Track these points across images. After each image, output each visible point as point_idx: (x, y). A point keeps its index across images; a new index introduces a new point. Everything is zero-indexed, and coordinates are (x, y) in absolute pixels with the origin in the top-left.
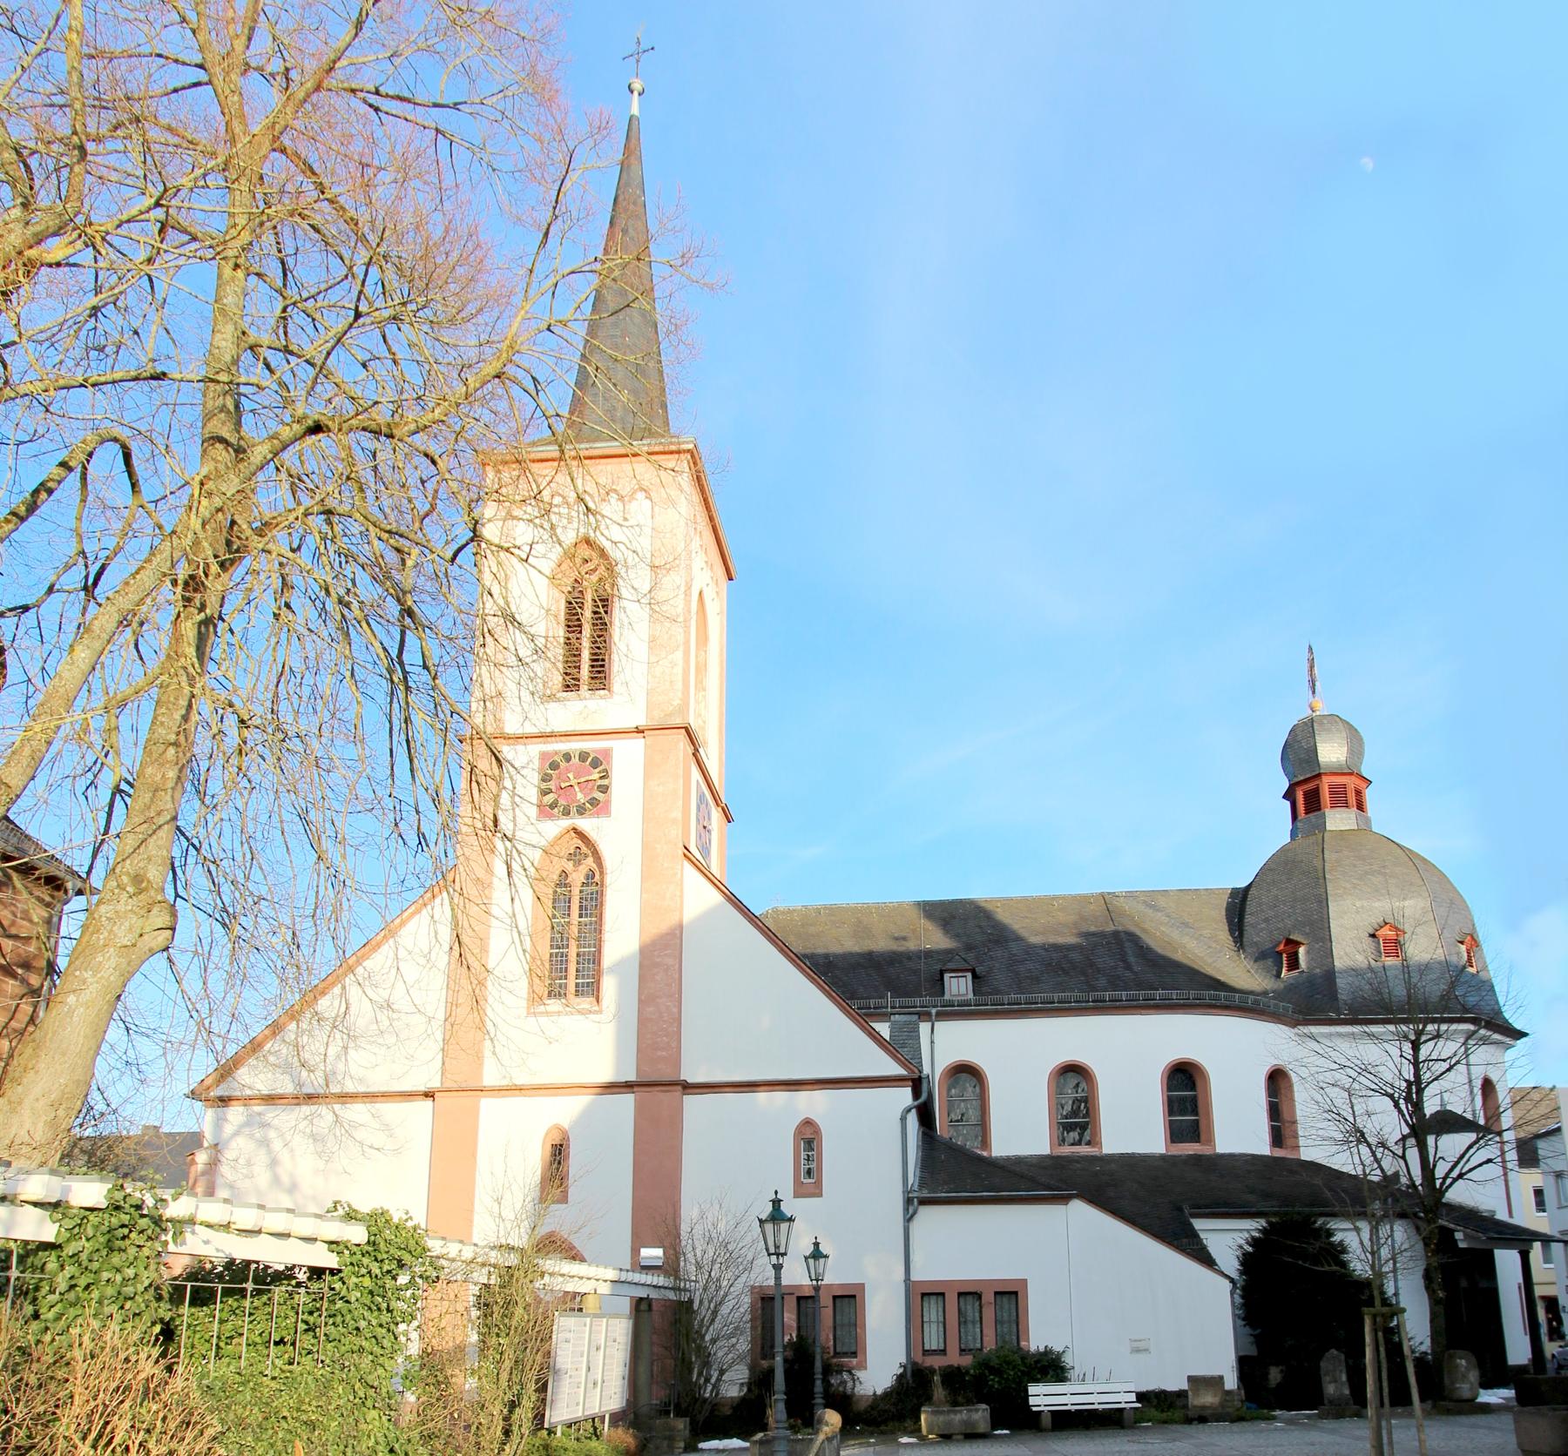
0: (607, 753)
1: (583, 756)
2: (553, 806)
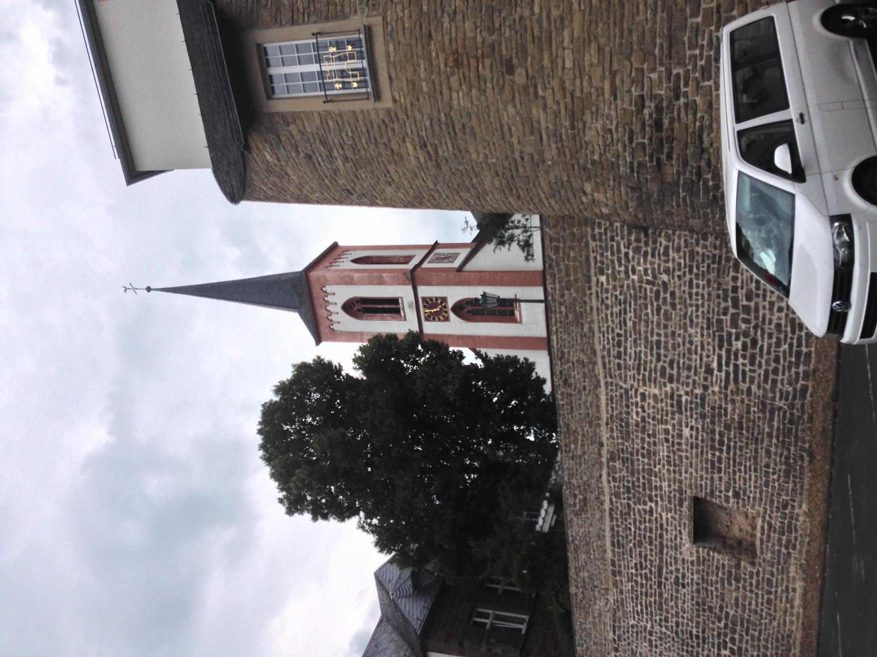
0: (424, 299)
1: (425, 307)
2: (444, 316)
